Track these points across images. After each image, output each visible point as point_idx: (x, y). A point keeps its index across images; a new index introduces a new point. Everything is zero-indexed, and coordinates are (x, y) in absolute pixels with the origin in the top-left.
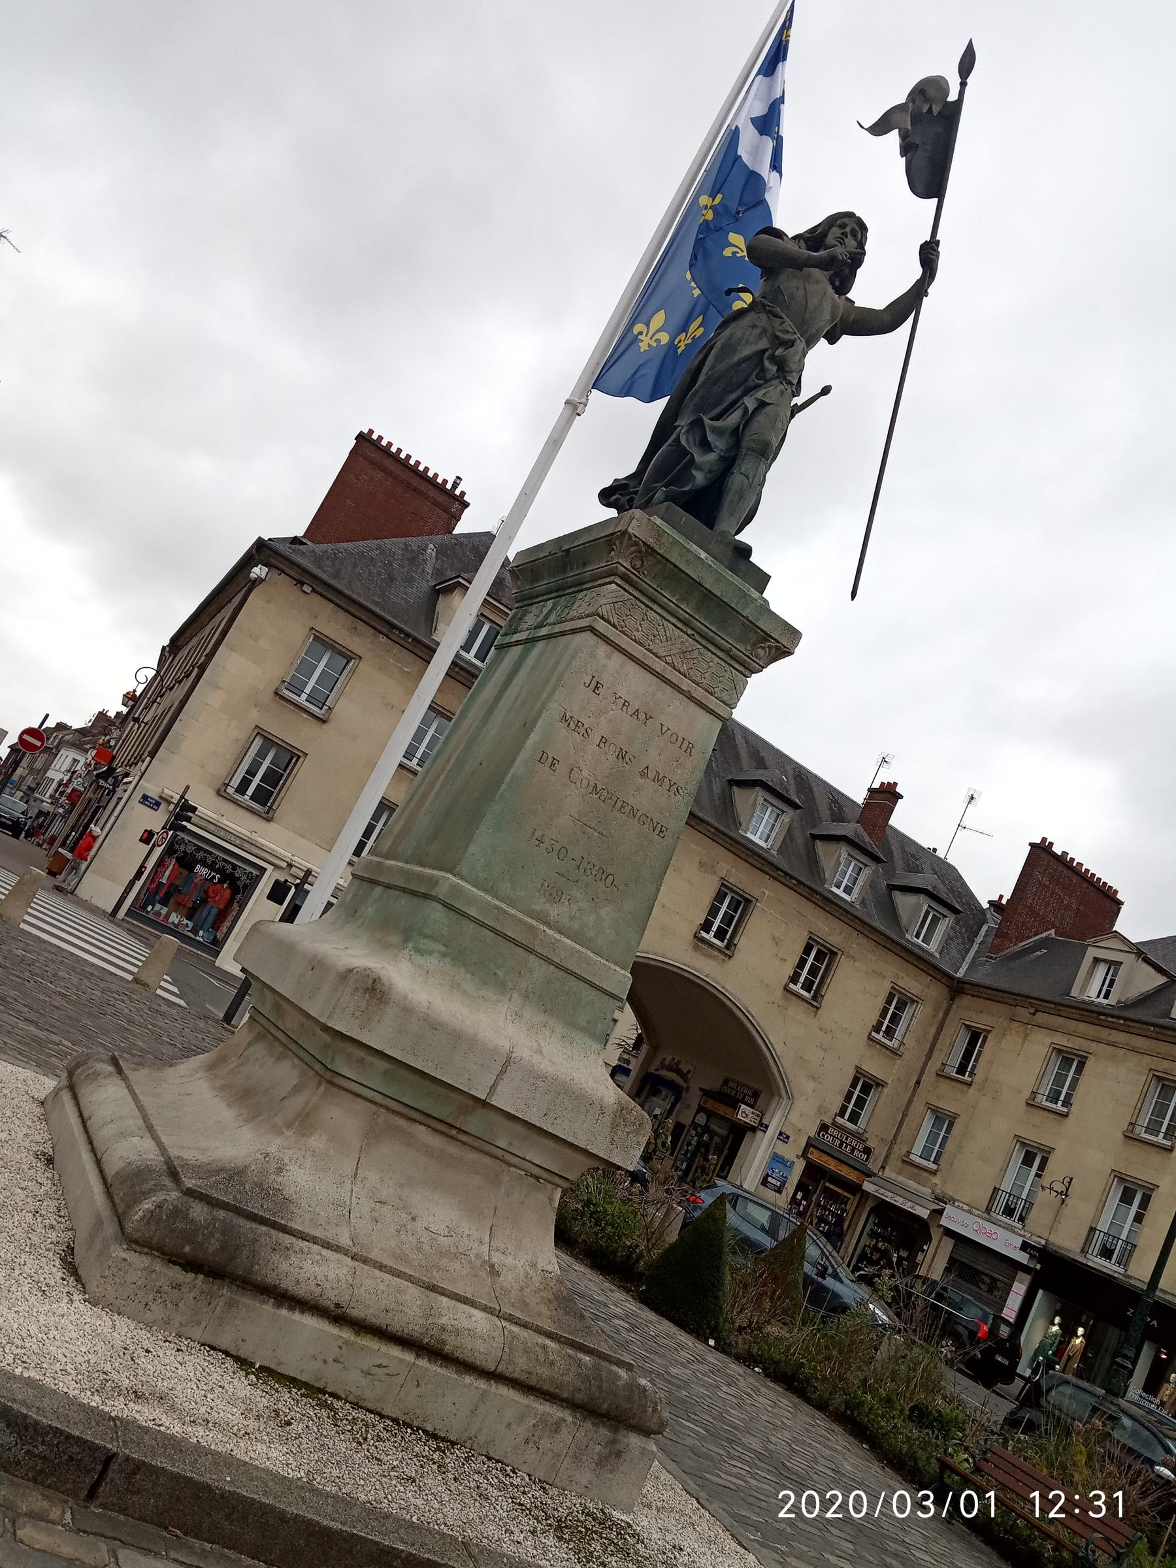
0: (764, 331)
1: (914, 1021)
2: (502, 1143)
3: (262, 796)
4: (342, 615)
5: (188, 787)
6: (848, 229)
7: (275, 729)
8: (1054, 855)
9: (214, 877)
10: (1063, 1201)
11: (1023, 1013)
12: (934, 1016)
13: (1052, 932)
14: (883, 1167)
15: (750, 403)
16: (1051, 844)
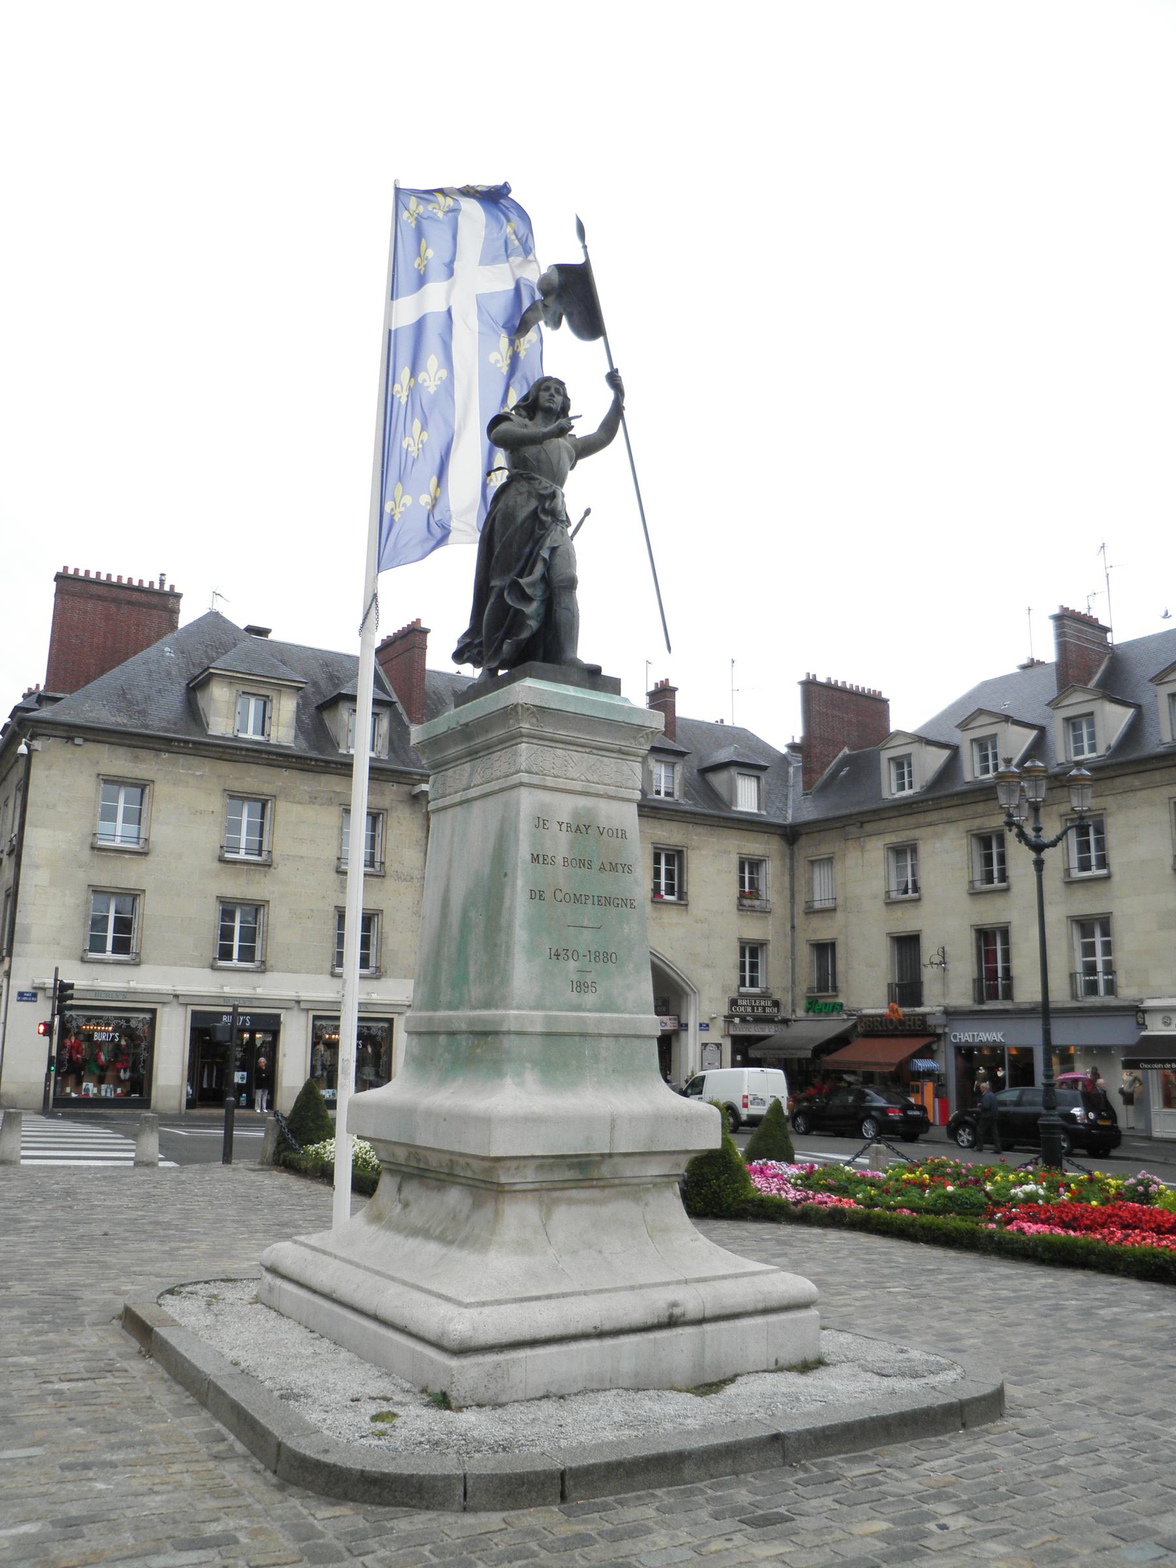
0: (530, 494)
1: (771, 877)
2: (628, 1174)
3: (122, 946)
4: (121, 751)
5: (57, 969)
6: (553, 391)
7: (105, 879)
8: (821, 685)
9: (114, 1037)
10: (944, 969)
11: (853, 830)
12: (783, 866)
13: (846, 750)
14: (794, 1011)
15: (545, 554)
16: (815, 676)
